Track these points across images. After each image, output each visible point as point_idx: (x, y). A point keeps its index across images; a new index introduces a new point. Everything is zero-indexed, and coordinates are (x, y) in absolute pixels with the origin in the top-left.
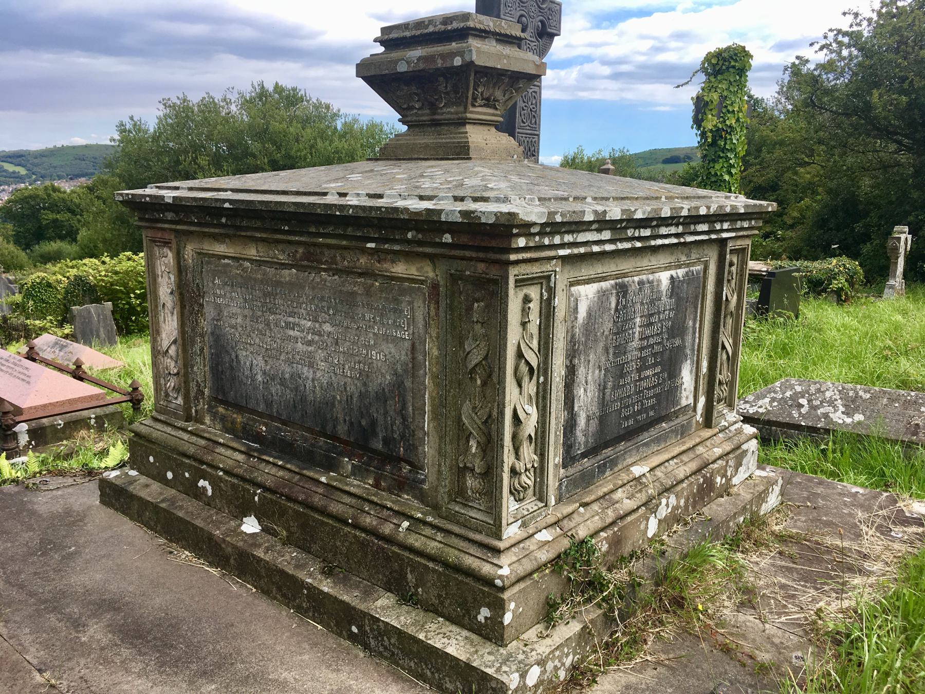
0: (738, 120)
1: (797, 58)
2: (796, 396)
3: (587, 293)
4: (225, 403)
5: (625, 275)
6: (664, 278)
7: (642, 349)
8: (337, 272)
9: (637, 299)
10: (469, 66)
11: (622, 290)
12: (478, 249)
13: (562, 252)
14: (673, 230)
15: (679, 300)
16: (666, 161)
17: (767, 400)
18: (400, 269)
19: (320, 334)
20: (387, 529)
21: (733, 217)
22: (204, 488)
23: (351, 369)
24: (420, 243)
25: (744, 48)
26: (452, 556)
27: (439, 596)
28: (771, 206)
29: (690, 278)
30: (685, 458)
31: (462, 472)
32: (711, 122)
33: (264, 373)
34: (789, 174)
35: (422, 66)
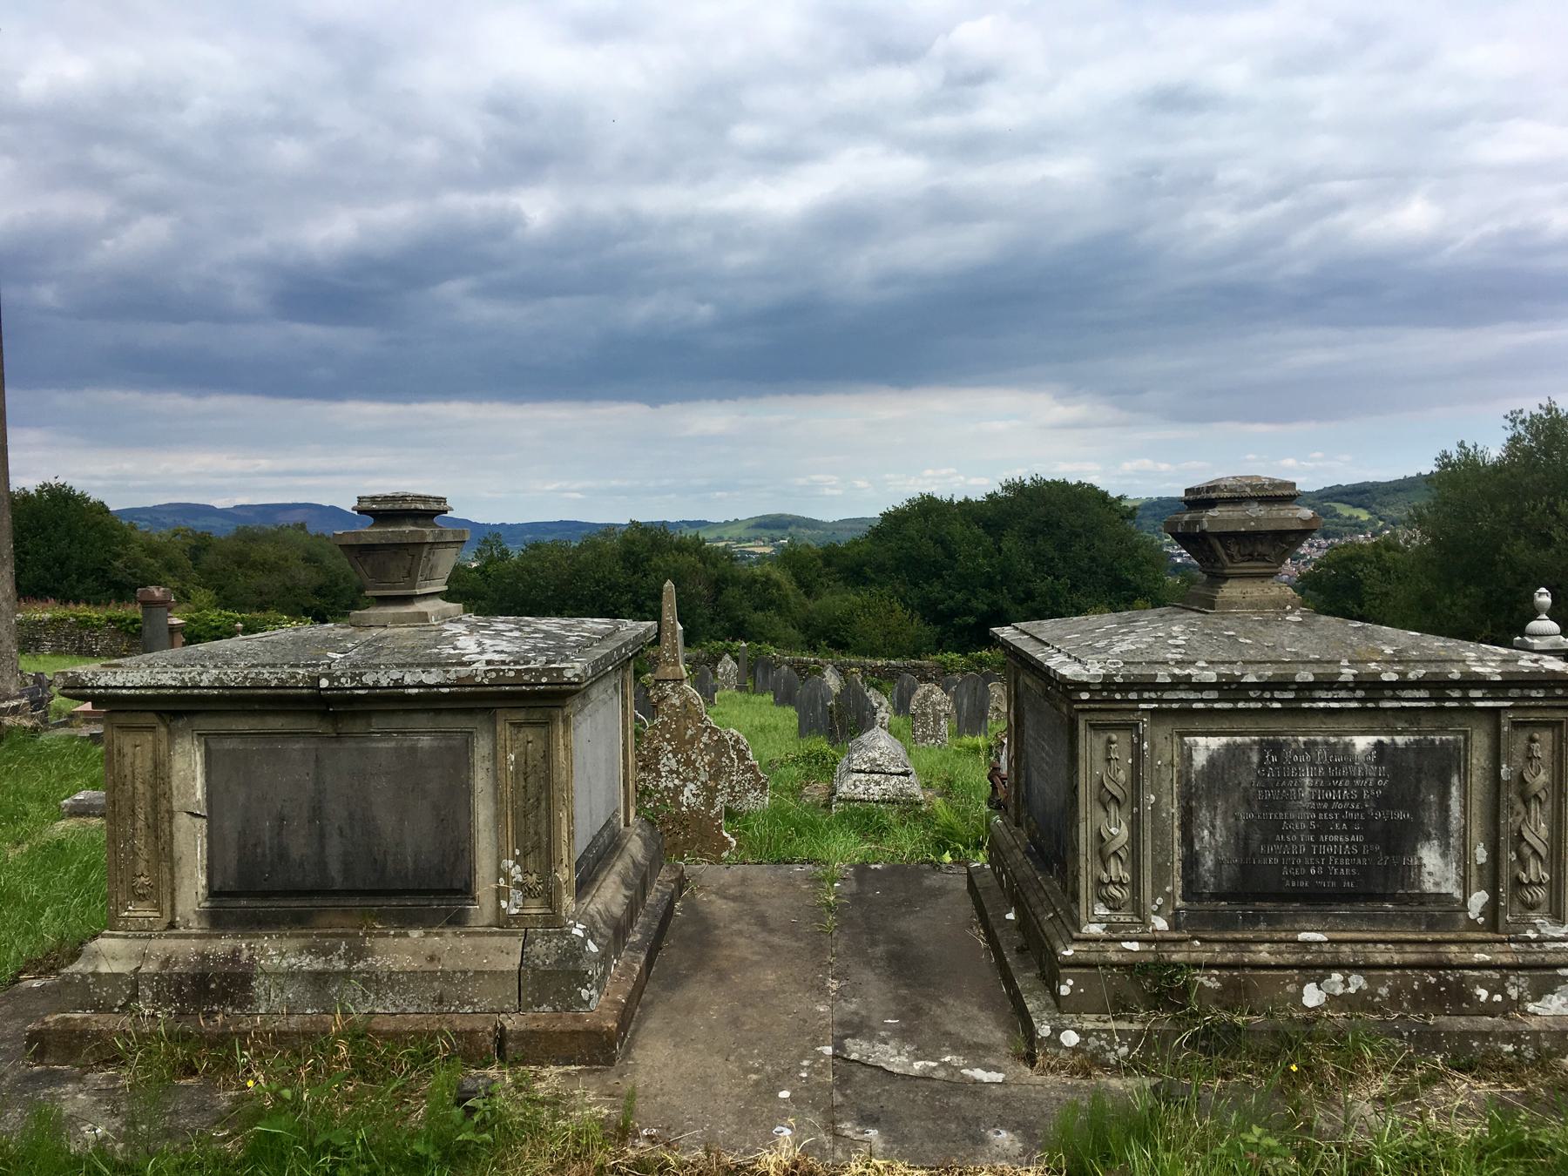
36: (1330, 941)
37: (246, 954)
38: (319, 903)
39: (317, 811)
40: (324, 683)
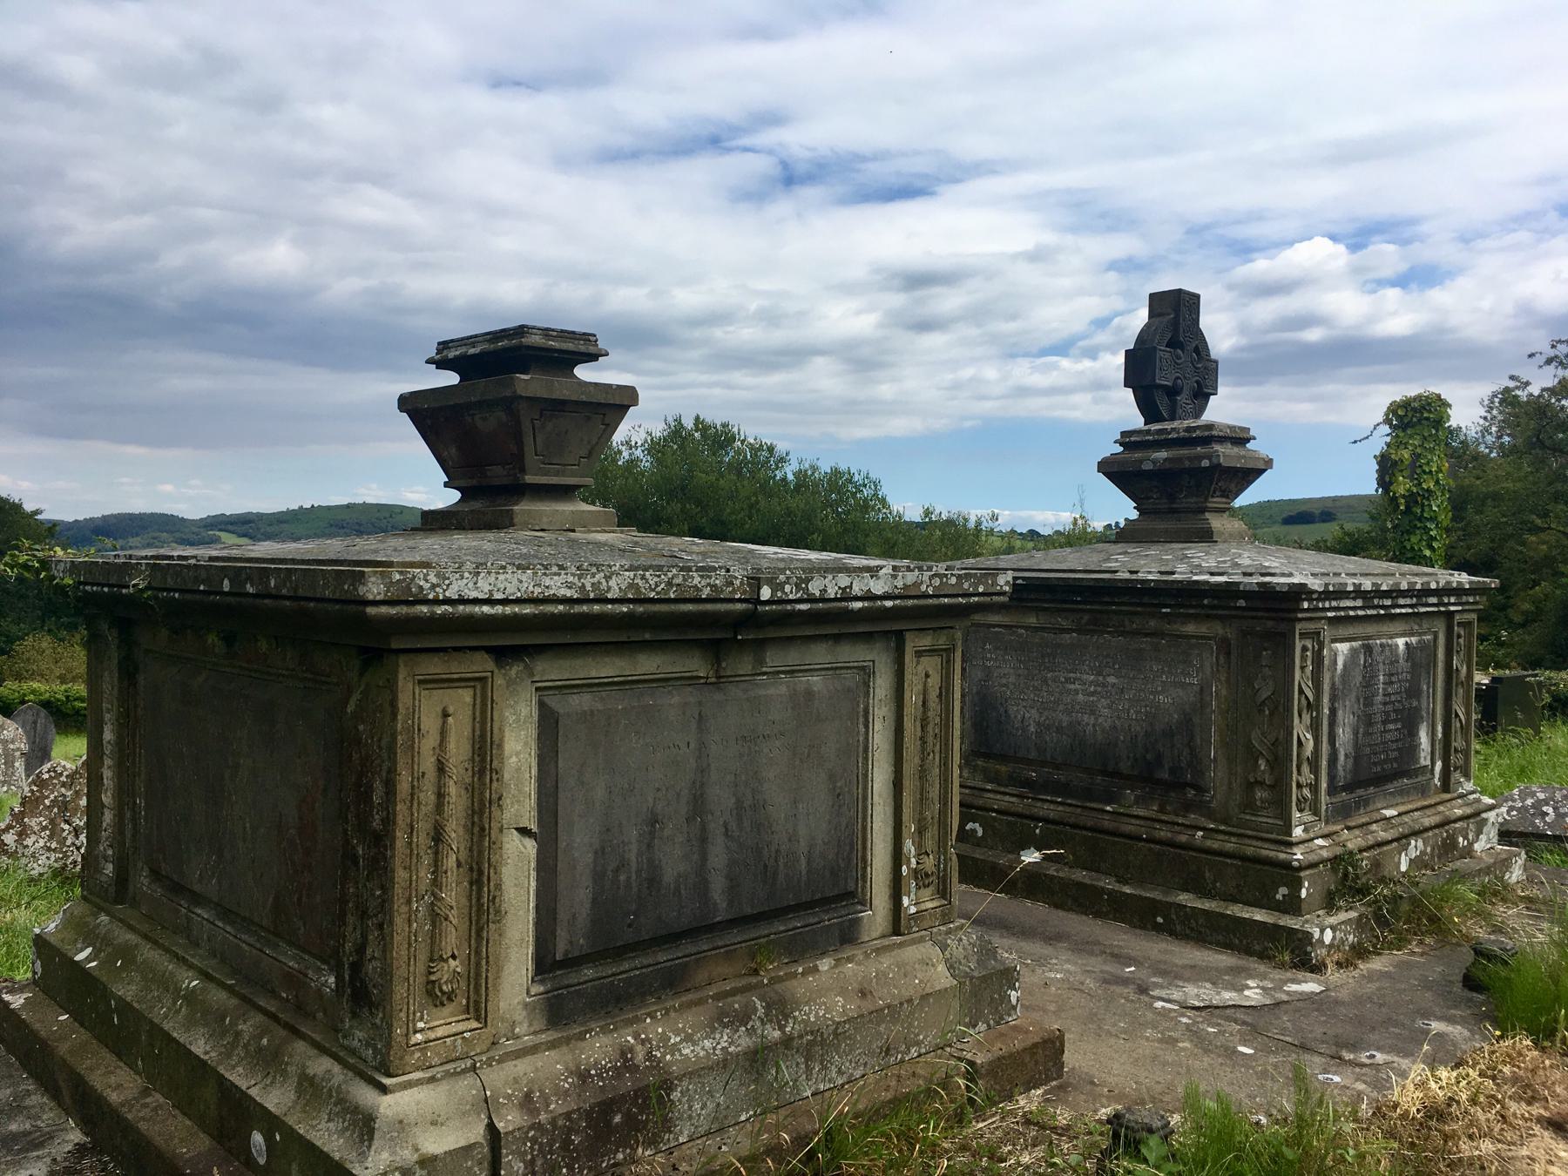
0: (1437, 482)
1: (1512, 378)
2: (1538, 804)
3: (1343, 648)
4: (987, 756)
5: (1369, 638)
6: (1401, 642)
7: (1385, 704)
8: (1123, 634)
9: (1380, 659)
10: (1216, 468)
11: (1368, 649)
12: (1267, 610)
13: (1330, 614)
14: (1408, 601)
15: (1414, 665)
16: (1289, 521)
17: (1504, 809)
18: (1190, 628)
19: (1104, 685)
20: (1183, 838)
21: (1459, 591)
22: (974, 831)
23: (1137, 713)
24: (1213, 607)
25: (1439, 396)
26: (1250, 851)
27: (1238, 886)
28: (1494, 583)
29: (1422, 646)
30: (1428, 812)
31: (1250, 786)
32: (1402, 486)
33: (1038, 724)
34: (1511, 543)
35: (1168, 465)
36: (1400, 815)
37: (640, 1055)
38: (692, 949)
39: (698, 805)
40: (766, 593)
